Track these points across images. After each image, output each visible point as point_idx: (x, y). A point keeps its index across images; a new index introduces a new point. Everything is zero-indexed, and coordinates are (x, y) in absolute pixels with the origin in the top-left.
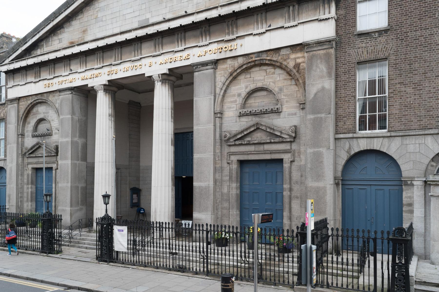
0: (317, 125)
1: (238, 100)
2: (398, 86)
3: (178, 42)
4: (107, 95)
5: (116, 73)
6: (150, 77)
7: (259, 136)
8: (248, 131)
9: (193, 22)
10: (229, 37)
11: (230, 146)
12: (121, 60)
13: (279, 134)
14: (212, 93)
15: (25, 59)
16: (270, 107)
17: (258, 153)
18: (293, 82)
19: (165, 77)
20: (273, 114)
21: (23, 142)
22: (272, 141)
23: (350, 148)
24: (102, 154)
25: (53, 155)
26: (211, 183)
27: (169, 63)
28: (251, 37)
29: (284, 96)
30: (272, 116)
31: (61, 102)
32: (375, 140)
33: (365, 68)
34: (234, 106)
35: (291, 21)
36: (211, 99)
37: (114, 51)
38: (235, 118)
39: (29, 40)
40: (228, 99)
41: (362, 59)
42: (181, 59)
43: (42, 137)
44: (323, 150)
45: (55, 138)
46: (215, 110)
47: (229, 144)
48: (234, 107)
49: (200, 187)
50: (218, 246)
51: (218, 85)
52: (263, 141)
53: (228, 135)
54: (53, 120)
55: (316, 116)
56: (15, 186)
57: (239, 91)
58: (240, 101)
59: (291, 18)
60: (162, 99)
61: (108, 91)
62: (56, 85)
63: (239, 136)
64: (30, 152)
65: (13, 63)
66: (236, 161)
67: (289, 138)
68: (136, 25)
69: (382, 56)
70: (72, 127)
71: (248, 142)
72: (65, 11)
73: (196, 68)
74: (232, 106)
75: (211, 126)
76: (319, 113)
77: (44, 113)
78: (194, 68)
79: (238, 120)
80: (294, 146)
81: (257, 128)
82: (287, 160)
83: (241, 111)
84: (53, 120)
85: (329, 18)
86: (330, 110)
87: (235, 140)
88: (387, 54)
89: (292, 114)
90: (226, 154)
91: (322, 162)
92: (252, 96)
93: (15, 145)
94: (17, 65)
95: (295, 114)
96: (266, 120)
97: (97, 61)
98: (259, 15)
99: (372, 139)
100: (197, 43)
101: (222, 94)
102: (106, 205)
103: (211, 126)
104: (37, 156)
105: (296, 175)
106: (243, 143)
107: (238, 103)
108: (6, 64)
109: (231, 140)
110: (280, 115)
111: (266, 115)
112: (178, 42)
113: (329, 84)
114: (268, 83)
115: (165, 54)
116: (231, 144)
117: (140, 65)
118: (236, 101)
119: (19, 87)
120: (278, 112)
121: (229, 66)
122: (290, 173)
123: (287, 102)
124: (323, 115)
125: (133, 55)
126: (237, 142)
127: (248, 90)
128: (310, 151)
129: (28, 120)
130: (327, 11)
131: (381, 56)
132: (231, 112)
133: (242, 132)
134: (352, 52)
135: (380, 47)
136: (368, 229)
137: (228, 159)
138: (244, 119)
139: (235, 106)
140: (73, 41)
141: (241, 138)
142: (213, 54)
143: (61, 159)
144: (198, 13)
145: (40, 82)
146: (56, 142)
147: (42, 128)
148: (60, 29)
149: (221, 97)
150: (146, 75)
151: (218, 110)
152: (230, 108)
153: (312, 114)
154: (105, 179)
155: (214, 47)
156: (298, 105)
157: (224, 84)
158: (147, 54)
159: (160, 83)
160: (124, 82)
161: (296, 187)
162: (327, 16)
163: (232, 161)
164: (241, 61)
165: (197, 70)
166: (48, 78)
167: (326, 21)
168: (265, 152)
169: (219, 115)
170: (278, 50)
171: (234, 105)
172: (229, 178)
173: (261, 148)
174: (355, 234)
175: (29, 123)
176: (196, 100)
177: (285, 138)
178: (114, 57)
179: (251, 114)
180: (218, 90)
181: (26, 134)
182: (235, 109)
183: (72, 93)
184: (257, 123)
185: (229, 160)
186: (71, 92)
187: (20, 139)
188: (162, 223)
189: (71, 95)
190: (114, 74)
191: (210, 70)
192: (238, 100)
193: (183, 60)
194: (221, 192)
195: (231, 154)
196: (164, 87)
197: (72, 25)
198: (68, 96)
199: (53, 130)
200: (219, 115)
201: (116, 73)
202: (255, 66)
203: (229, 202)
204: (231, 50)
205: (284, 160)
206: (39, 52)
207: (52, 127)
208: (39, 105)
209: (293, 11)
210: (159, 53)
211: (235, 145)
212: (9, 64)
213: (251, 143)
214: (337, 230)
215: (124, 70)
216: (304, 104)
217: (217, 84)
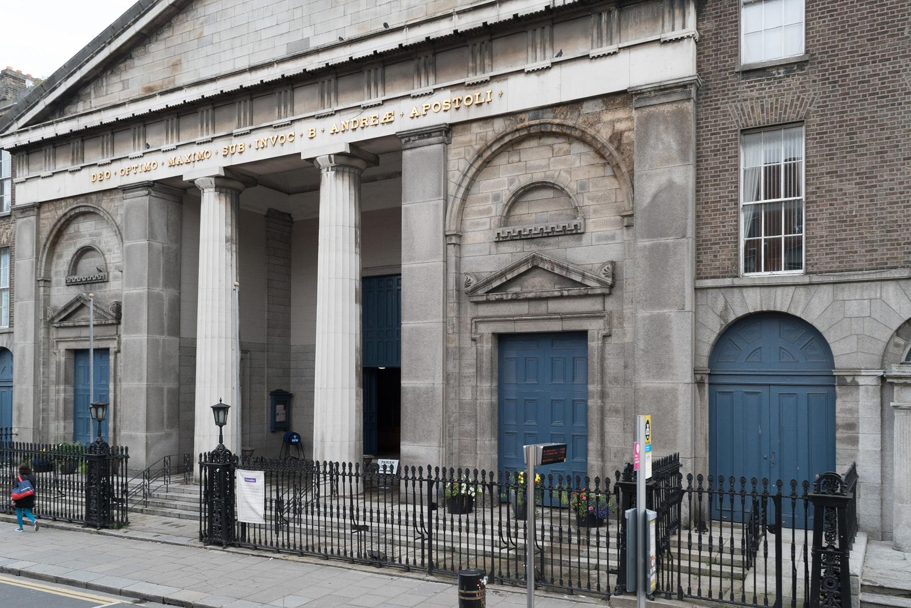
0: (659, 260)
1: (494, 207)
2: (827, 178)
3: (474, 61)
4: (223, 198)
5: (241, 153)
6: (312, 160)
7: (537, 284)
8: (516, 273)
9: (401, 45)
10: (476, 77)
11: (477, 303)
13: (578, 279)
14: (440, 195)
15: (52, 124)
16: (560, 223)
17: (537, 318)
18: (609, 171)
19: (342, 160)
21: (49, 295)
22: (565, 293)
23: (726, 309)
24: (212, 321)
25: (110, 322)
26: (439, 382)
27: (350, 131)
28: (521, 78)
30: (566, 241)
32: (779, 291)
33: (758, 142)
35: (604, 44)
36: (437, 205)
37: (366, 73)
38: (488, 246)
40: (473, 207)
41: (751, 123)
43: (88, 286)
44: (671, 313)
45: (115, 288)
46: (447, 229)
47: (475, 299)
48: (484, 224)
49: (414, 389)
50: (452, 512)
52: (545, 294)
53: (474, 282)
54: (109, 251)
55: (655, 241)
56: (31, 388)
57: (496, 190)
58: (497, 209)
59: (604, 38)
60: (336, 207)
61: (224, 190)
64: (63, 316)
66: (490, 335)
68: (282, 53)
69: (793, 117)
71: (515, 297)
72: (134, 22)
73: (406, 142)
75: (439, 263)
76: (661, 235)
77: (91, 235)
78: (403, 141)
79: (493, 249)
80: (611, 304)
81: (534, 266)
82: (596, 332)
83: (500, 230)
84: (109, 251)
85: (682, 38)
87: (488, 292)
88: (803, 113)
89: (607, 238)
90: (469, 321)
91: (668, 337)
92: (524, 199)
93: (31, 303)
94: (35, 136)
95: (613, 237)
96: (552, 251)
97: (202, 127)
98: (538, 32)
99: (773, 290)
100: (408, 89)
101: (460, 195)
102: (221, 427)
105: (613, 364)
106: (505, 297)
107: (493, 214)
108: (12, 134)
109: (480, 292)
110: (580, 240)
111: (552, 240)
113: (683, 176)
114: (557, 174)
115: (342, 113)
116: (480, 299)
118: (489, 211)
119: (40, 180)
121: (475, 137)
122: (602, 359)
123: (595, 212)
124: (670, 240)
125: (277, 115)
126: (493, 297)
127: (515, 187)
129: (59, 249)
130: (678, 23)
131: (791, 116)
132: (479, 232)
133: (503, 274)
134: (730, 107)
135: (788, 98)
137: (473, 331)
138: (507, 248)
140: (151, 85)
141: (500, 288)
143: (126, 331)
144: (411, 26)
145: (83, 171)
147: (88, 266)
148: (125, 61)
149: (458, 201)
150: (303, 157)
151: (452, 228)
152: (478, 224)
155: (445, 97)
158: (305, 112)
160: (257, 170)
161: (613, 390)
162: (678, 33)
163: (482, 335)
164: (499, 126)
165: (409, 146)
168: (550, 317)
170: (576, 104)
171: (485, 219)
173: (542, 308)
174: (737, 488)
175: (60, 256)
176: (406, 209)
177: (592, 288)
179: (520, 237)
181: (54, 279)
182: (487, 227)
183: (149, 194)
184: (534, 257)
186: (146, 192)
187: (42, 289)
188: (337, 464)
189: (147, 198)
190: (237, 154)
192: (494, 207)
195: (479, 321)
196: (340, 182)
197: (149, 53)
198: (141, 199)
200: (454, 239)
201: (241, 153)
202: (529, 137)
204: (481, 104)
206: (81, 108)
207: (109, 265)
208: (81, 218)
209: (609, 22)
210: (330, 110)
211: (488, 302)
214: (700, 478)
215: (257, 145)
216: (632, 215)
217: (450, 174)
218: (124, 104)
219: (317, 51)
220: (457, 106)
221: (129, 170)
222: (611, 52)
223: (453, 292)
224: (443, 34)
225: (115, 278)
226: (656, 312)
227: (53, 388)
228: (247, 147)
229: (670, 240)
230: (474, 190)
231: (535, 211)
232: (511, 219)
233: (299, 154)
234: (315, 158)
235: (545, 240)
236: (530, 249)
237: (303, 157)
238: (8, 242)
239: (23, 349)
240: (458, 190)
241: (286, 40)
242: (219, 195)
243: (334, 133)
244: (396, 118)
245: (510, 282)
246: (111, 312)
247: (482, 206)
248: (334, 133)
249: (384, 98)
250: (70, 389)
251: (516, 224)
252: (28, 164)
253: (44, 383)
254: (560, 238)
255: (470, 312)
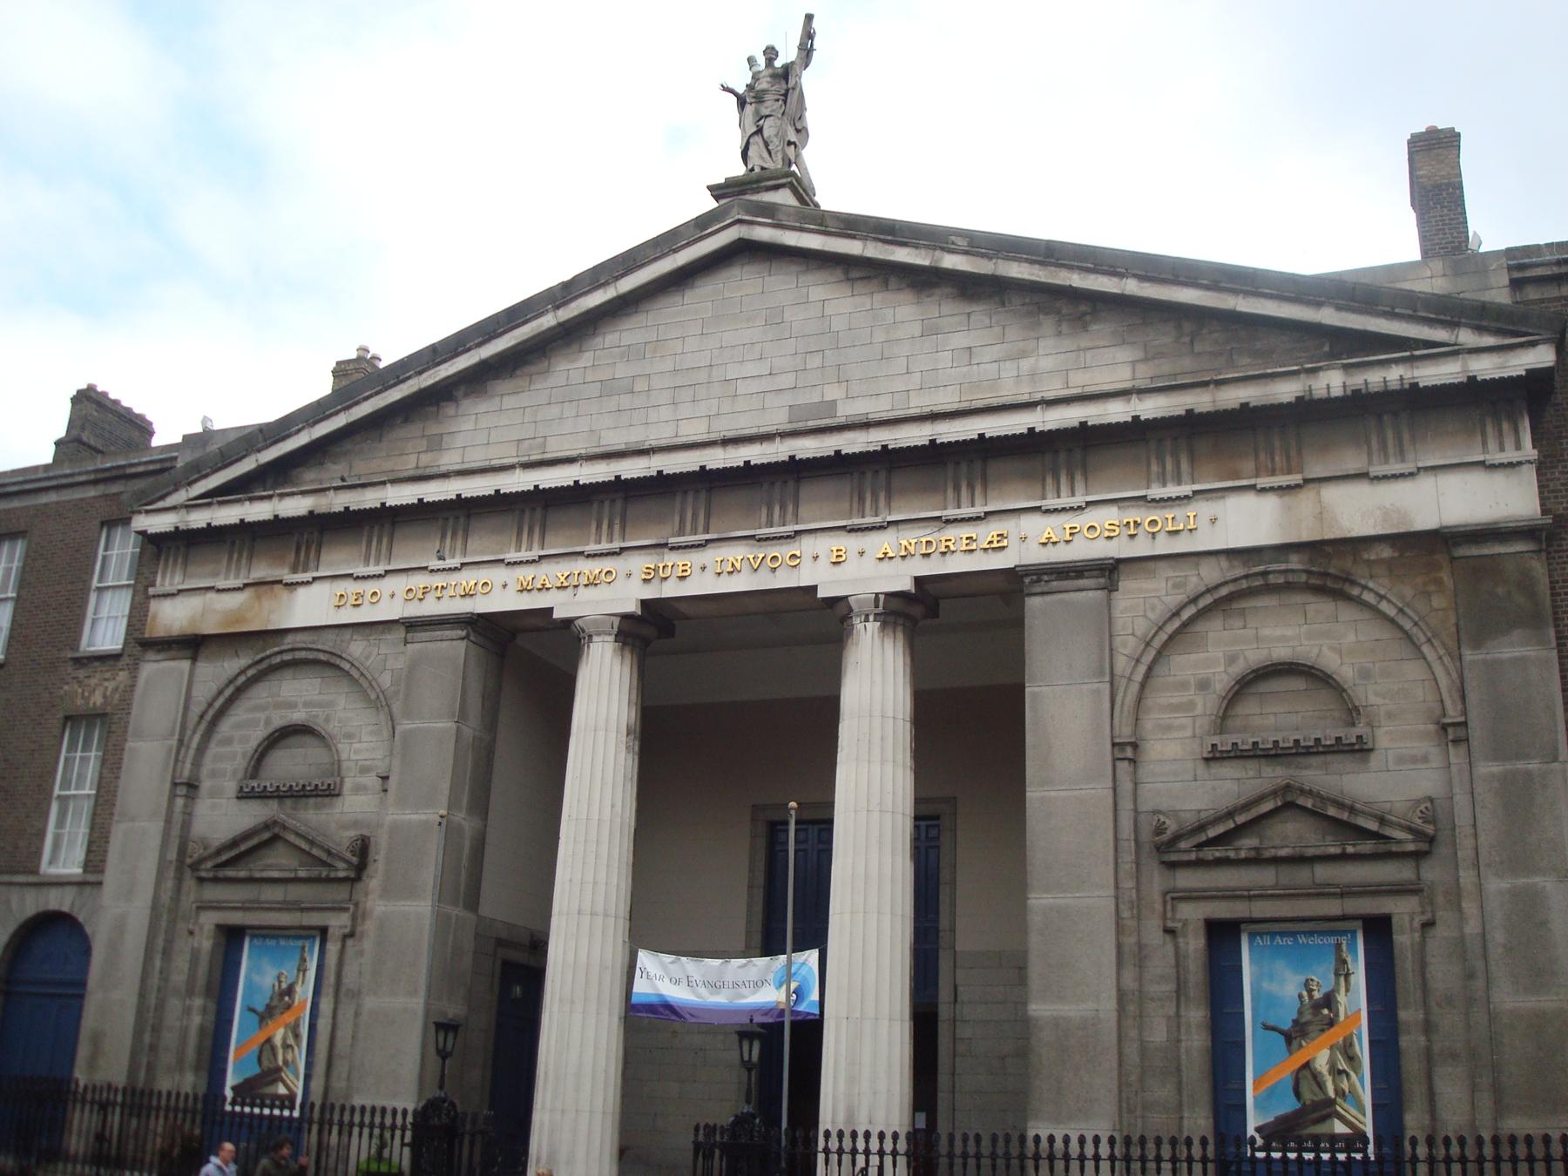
1: (1199, 701)
3: (957, 489)
4: (628, 656)
5: (682, 578)
6: (568, 623)
10: (957, 511)
11: (1173, 866)
12: (707, 531)
13: (1373, 826)
14: (1102, 674)
16: (1330, 733)
20: (1339, 757)
21: (190, 814)
22: (1350, 849)
24: (595, 883)
25: (341, 874)
26: (1108, 1006)
27: (918, 556)
29: (1377, 694)
30: (1336, 762)
31: (413, 666)
34: (1184, 721)
35: (1392, 460)
36: (1098, 691)
37: (595, 506)
38: (1190, 765)
39: (299, 431)
40: (1159, 698)
42: (974, 546)
43: (289, 802)
45: (356, 807)
46: (1117, 732)
47: (1173, 857)
48: (1182, 727)
51: (1124, 645)
52: (1310, 852)
53: (1172, 827)
54: (349, 736)
55: (1508, 766)
56: (133, 1000)
57: (1203, 673)
58: (1206, 705)
59: (1391, 451)
60: (875, 688)
61: (630, 640)
62: (391, 599)
63: (1212, 833)
64: (224, 857)
65: (209, 505)
66: (1201, 924)
67: (1413, 841)
68: (777, 419)
70: (454, 766)
71: (1252, 854)
72: (479, 345)
73: (1033, 582)
74: (1177, 722)
75: (1103, 789)
76: (1518, 756)
77: (306, 704)
78: (1027, 580)
80: (1432, 872)
81: (1288, 802)
82: (1407, 918)
83: (1216, 740)
84: (349, 736)
85: (1519, 463)
86: (1556, 749)
87: (1200, 846)
89: (1414, 760)
90: (1157, 898)
92: (1253, 690)
93: (155, 829)
94: (227, 515)
95: (1425, 759)
96: (1316, 776)
97: (599, 527)
98: (964, 467)
100: (1034, 499)
101: (1139, 677)
102: (444, 1059)
103: (1101, 790)
104: (257, 875)
105: (1443, 974)
106: (1232, 854)
107: (1199, 710)
109: (1183, 845)
110: (1366, 761)
111: (1314, 760)
112: (957, 489)
114: (1316, 651)
116: (1185, 857)
117: (793, 556)
118: (1190, 706)
120: (1361, 750)
122: (1423, 965)
123: (1390, 715)
124: (1534, 765)
125: (764, 519)
126: (1210, 853)
127: (1239, 668)
128: (1496, 885)
130: (1509, 442)
132: (1172, 748)
133: (1230, 814)
136: (1185, 1135)
137: (1169, 915)
138: (1229, 770)
139: (1189, 721)
141: (240, 854)
142: (1102, 543)
143: (386, 893)
145: (316, 587)
146: (355, 824)
147: (290, 765)
149: (1135, 688)
150: (821, 594)
151: (1125, 734)
152: (1169, 728)
153: (1495, 759)
154: (600, 983)
155: (1107, 517)
156: (1432, 727)
157: (1148, 644)
158: (822, 519)
159: (873, 626)
161: (1449, 1020)
162: (1510, 455)
163: (1185, 923)
164: (1211, 573)
165: (1037, 589)
166: (361, 570)
167: (1509, 471)
169: (1129, 753)
171: (1182, 719)
172: (1172, 987)
173: (1302, 875)
177: (1400, 842)
178: (677, 518)
179: (1256, 754)
180: (1122, 664)
181: (206, 784)
182: (1189, 733)
183: (467, 637)
184: (1288, 786)
185: (1173, 919)
186: (464, 633)
187: (180, 802)
189: (463, 644)
190: (673, 580)
191: (1091, 594)
193: (978, 554)
194: (1142, 1042)
195: (1176, 897)
196: (889, 643)
198: (454, 649)
199: (343, 773)
200: (1127, 751)
201: (682, 578)
202: (1269, 589)
203: (1180, 1083)
204: (1177, 532)
205: (1394, 920)
207: (345, 765)
208: (288, 673)
210: (878, 519)
211: (1200, 863)
212: (187, 507)
213: (1267, 854)
215: (717, 569)
216: (1465, 724)
217: (1117, 641)
218: (511, 467)
219: (866, 425)
220: (1132, 532)
221: (426, 590)
222: (1407, 471)
223: (1128, 846)
224: (1114, 419)
225: (358, 789)
226: (1522, 881)
227: (174, 1005)
228: (696, 569)
229: (1534, 765)
230: (1160, 670)
231: (1275, 710)
232: (1230, 723)
233: (814, 588)
234: (846, 597)
235: (1300, 759)
236: (1274, 775)
237: (556, 615)
238: (105, 703)
239: (120, 926)
240: (1135, 666)
241: (788, 399)
242: (622, 649)
243: (885, 557)
244: (806, 562)
245: (1239, 830)
246: (348, 855)
247: (1176, 698)
248: (885, 557)
249: (542, 553)
250: (212, 1006)
251: (1244, 729)
252: (185, 564)
253: (159, 989)
254: (1329, 758)
255: (191, 892)
